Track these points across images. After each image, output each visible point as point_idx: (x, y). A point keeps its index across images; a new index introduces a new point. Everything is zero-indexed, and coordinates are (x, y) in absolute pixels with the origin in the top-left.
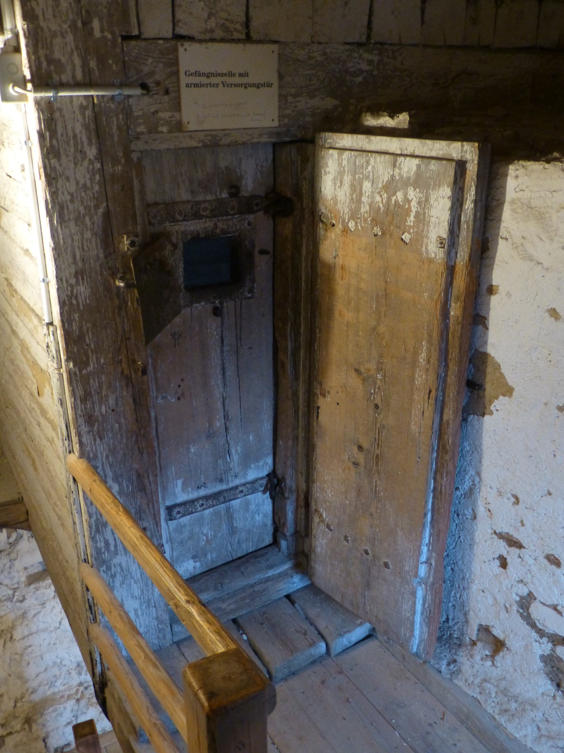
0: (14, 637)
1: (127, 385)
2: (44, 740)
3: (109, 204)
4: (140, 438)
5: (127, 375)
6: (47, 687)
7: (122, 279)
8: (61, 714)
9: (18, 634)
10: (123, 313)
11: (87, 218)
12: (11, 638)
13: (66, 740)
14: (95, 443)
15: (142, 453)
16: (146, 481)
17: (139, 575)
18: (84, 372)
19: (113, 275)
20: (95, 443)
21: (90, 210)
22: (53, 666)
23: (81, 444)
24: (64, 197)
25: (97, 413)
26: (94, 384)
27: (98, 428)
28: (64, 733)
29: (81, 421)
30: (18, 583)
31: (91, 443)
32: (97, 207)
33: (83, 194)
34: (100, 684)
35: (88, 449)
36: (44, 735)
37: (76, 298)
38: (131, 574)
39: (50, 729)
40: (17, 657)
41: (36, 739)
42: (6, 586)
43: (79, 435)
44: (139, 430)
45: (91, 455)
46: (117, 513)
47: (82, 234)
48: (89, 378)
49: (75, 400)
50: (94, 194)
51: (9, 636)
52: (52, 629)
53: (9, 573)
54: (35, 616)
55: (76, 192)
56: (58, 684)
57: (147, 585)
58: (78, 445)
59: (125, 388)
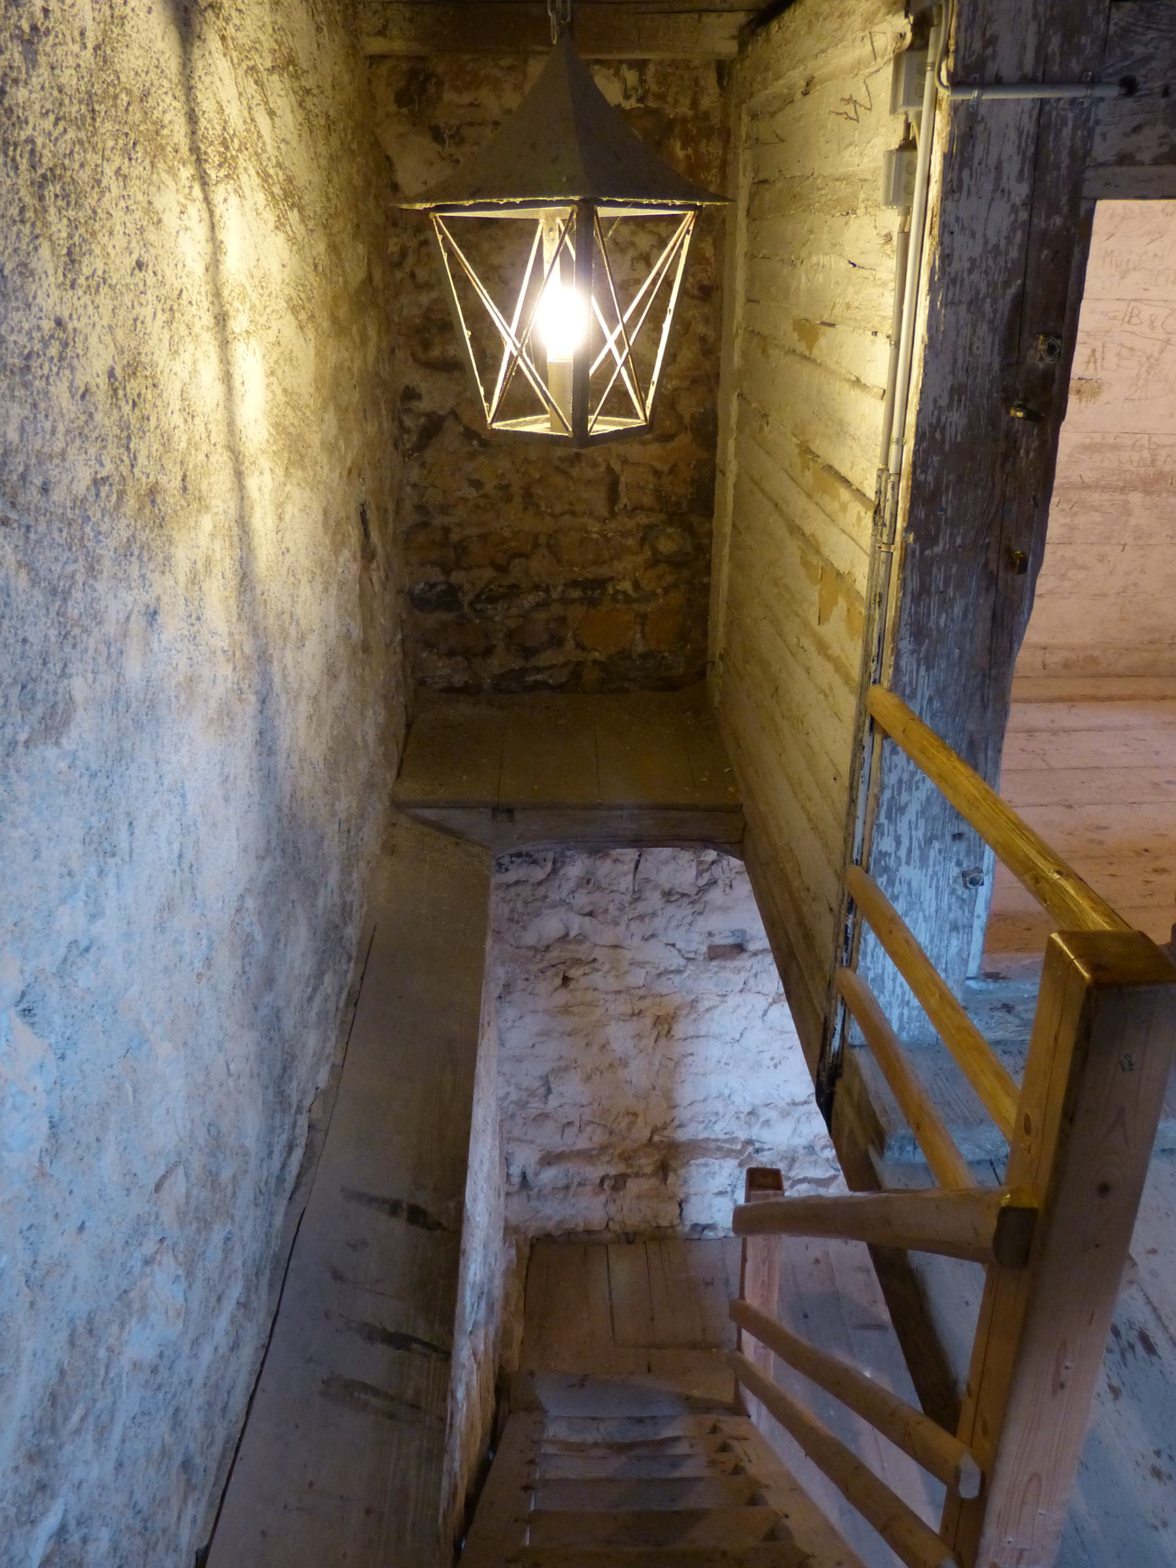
0: (672, 1033)
1: (988, 589)
2: (680, 1205)
3: (1028, 282)
4: (987, 681)
5: (992, 572)
6: (701, 1127)
7: (1021, 407)
8: (714, 1173)
9: (679, 1030)
10: (1008, 466)
11: (988, 301)
12: (669, 1032)
13: (712, 1218)
14: (918, 672)
15: (985, 707)
16: (981, 756)
17: (933, 909)
18: (928, 552)
19: (1008, 402)
20: (918, 672)
21: (995, 288)
22: (717, 1098)
23: (897, 668)
24: (960, 265)
25: (932, 625)
26: (938, 576)
27: (928, 651)
28: (710, 1205)
29: (905, 631)
30: (696, 952)
31: (911, 672)
32: (1007, 284)
33: (991, 262)
34: (830, 1069)
35: (906, 679)
36: (682, 1196)
37: (943, 429)
38: (921, 903)
39: (692, 1190)
40: (671, 1064)
41: (671, 1198)
42: (679, 951)
43: (897, 653)
44: (990, 668)
45: (908, 691)
46: (948, 759)
47: (974, 327)
48: (932, 565)
49: (904, 595)
50: (1006, 262)
51: (666, 1027)
52: (728, 1039)
53: (687, 931)
54: (708, 1010)
55: (981, 257)
56: (718, 1127)
57: (941, 931)
58: (891, 671)
59: (984, 592)
